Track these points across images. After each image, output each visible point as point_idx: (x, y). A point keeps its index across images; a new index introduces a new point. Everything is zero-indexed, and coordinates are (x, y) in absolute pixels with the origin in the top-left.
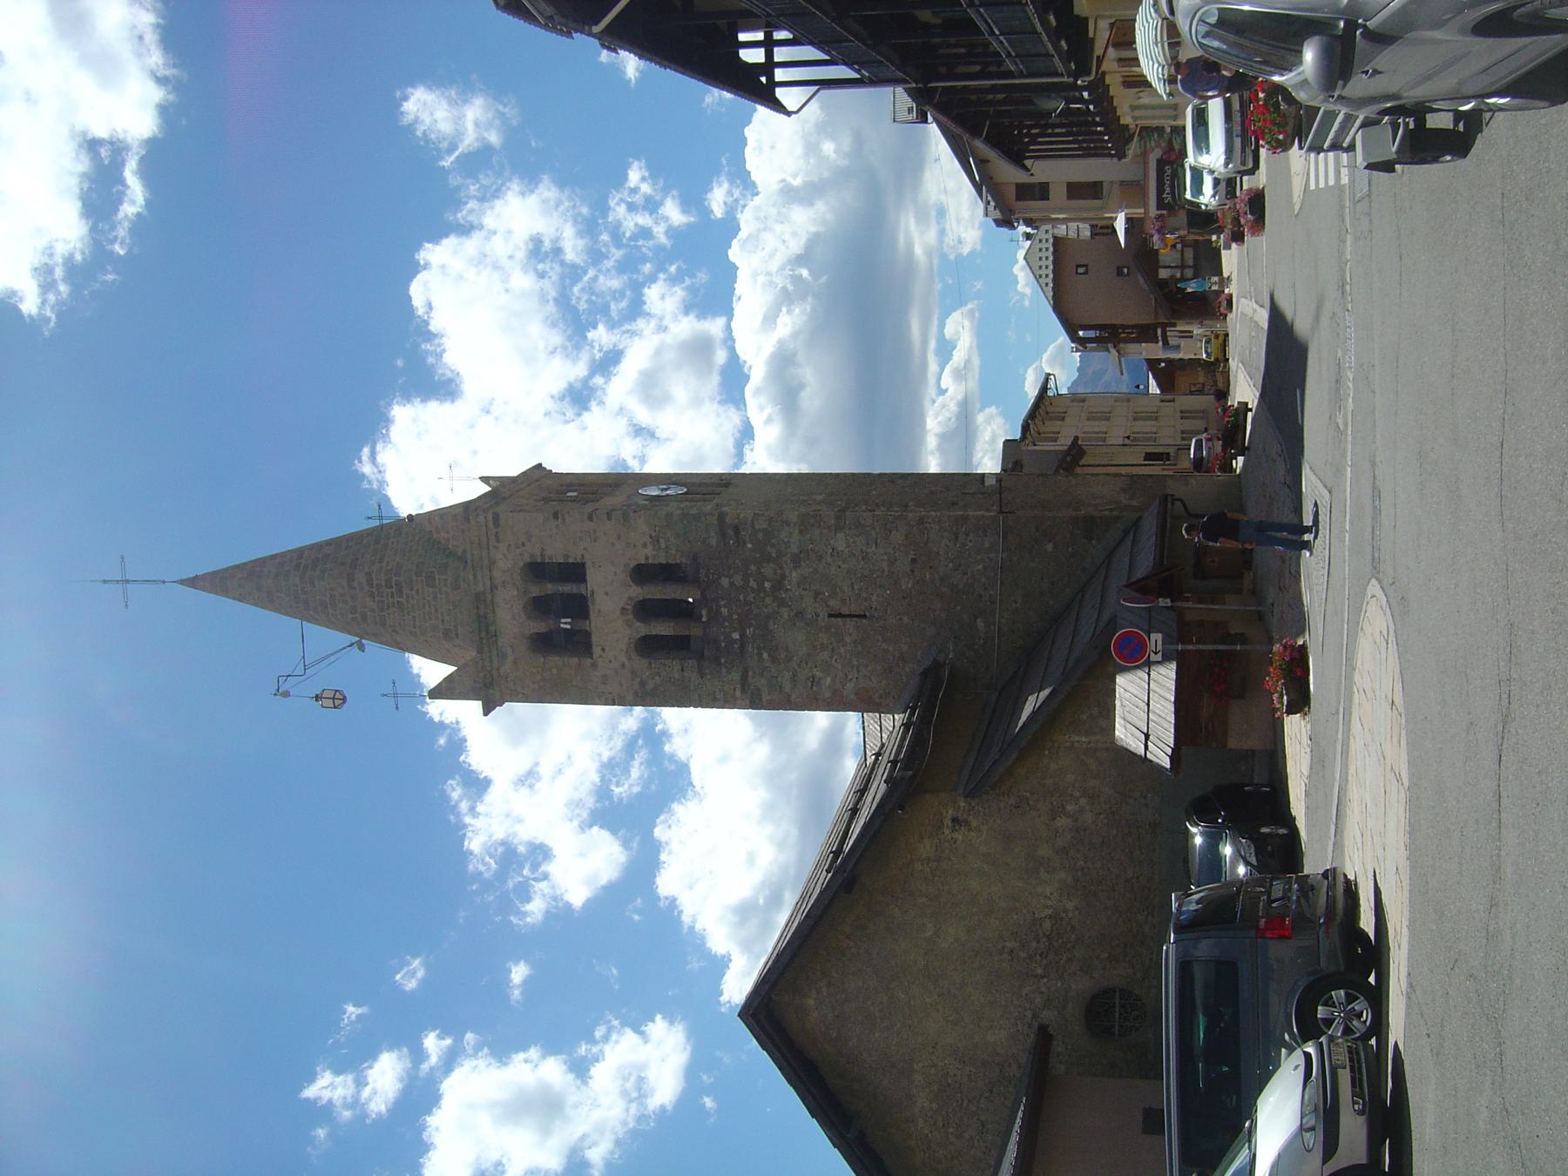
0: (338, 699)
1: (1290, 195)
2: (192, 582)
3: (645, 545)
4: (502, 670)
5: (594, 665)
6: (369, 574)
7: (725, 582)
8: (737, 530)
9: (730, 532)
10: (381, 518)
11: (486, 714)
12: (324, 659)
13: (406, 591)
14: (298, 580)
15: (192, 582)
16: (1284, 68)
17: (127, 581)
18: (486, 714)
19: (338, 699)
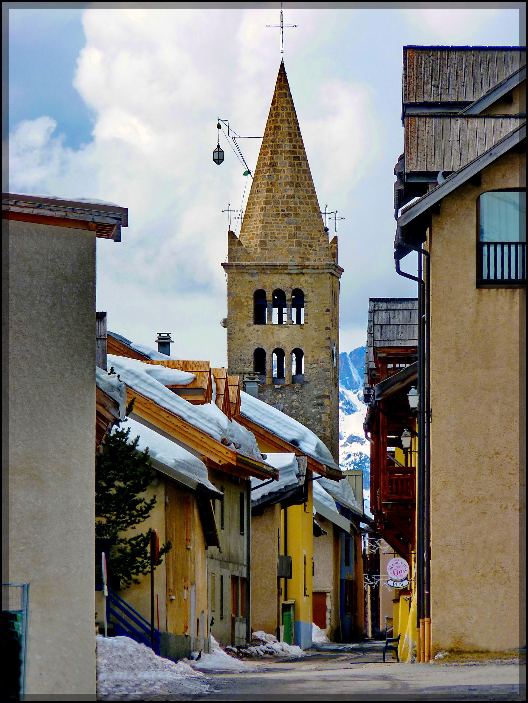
0: (219, 160)
1: (213, 491)
2: (282, 65)
3: (313, 357)
4: (246, 275)
5: (249, 325)
6: (293, 197)
7: (295, 397)
8: (321, 404)
9: (320, 401)
10: (326, 213)
11: (222, 264)
12: (238, 149)
13: (286, 219)
14: (288, 149)
15: (282, 65)
16: (143, 479)
17: (282, 27)
18: (222, 264)
19: (219, 160)
